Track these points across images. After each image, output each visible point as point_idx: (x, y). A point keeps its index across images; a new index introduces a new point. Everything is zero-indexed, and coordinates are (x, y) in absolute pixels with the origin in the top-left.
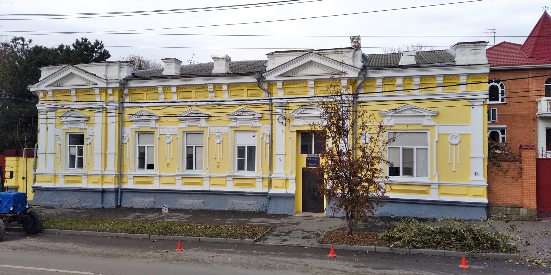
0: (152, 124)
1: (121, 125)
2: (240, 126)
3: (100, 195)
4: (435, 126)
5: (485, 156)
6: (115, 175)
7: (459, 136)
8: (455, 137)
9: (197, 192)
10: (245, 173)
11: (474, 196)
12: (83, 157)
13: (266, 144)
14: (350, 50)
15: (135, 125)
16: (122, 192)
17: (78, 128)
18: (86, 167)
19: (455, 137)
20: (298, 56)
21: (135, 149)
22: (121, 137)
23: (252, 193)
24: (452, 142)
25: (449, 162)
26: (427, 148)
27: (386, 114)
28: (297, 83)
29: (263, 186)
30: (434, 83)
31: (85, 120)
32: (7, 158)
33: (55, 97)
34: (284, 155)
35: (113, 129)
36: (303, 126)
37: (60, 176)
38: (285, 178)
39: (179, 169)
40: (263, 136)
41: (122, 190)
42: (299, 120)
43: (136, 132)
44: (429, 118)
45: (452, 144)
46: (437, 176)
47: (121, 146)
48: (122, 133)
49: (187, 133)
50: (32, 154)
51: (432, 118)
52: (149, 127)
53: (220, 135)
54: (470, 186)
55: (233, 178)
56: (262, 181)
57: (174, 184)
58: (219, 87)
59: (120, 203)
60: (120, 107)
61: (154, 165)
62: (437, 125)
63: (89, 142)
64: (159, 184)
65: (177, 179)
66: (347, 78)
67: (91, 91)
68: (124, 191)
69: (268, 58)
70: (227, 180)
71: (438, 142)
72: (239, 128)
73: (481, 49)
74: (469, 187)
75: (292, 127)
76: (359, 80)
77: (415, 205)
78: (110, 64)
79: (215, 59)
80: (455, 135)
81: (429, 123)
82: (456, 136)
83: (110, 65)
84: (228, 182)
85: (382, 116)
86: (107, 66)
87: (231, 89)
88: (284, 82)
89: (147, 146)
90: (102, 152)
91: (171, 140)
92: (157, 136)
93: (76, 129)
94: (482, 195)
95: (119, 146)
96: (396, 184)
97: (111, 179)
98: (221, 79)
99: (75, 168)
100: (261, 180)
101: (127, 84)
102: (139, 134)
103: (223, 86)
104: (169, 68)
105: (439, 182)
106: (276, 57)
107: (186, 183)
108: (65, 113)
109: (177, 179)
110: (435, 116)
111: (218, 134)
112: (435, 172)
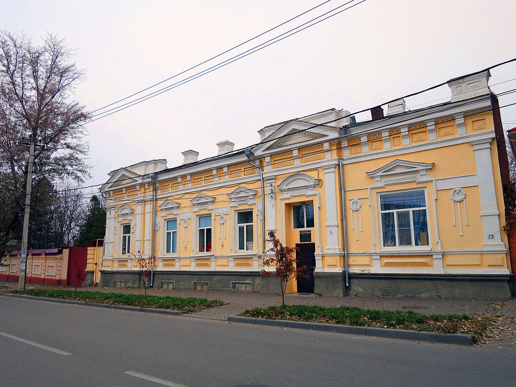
0: (174, 211)
1: (155, 213)
2: (386, 185)
3: (138, 276)
4: (432, 181)
5: (499, 212)
6: (340, 254)
7: (463, 190)
8: (458, 191)
9: (229, 274)
10: (205, 254)
11: (489, 266)
12: (311, 233)
13: (353, 212)
14: (331, 111)
15: (164, 213)
16: (154, 274)
17: (127, 219)
18: (320, 246)
19: (458, 191)
20: (276, 130)
21: (164, 235)
22: (155, 226)
23: (177, 272)
24: (455, 199)
25: (454, 225)
26: (176, 232)
27: (374, 174)
28: (240, 165)
29: (444, 265)
30: (241, 169)
31: (131, 213)
32: (88, 248)
33: (115, 196)
34: (337, 227)
35: (148, 217)
36: (291, 198)
37: (159, 261)
38: (441, 252)
39: (193, 251)
40: (258, 213)
41: (154, 273)
42: (287, 192)
43: (165, 220)
44: (424, 173)
45: (455, 202)
46: (439, 244)
47: (154, 232)
48: (155, 221)
49: (201, 217)
50: (101, 244)
51: (428, 172)
52: (172, 214)
53: (223, 216)
54: (371, 255)
55: (380, 256)
56: (443, 258)
57: (190, 265)
58: (243, 165)
59: (153, 285)
60: (153, 199)
61: (315, 243)
62: (434, 180)
63: (133, 232)
64: (216, 265)
65: (374, 259)
66: (408, 126)
67: (240, 165)
68: (156, 273)
69: (218, 146)
70: (373, 258)
71: (438, 201)
72: (385, 188)
73: (480, 81)
74: (372, 256)
75: (162, 217)
76: (343, 141)
77: (416, 281)
78: (148, 163)
79: (219, 145)
80: (458, 189)
81: (424, 179)
82: (459, 191)
83: (149, 164)
84: (374, 262)
85: (370, 177)
86: (147, 165)
87: (439, 127)
88: (271, 155)
89: (173, 232)
90: (338, 224)
91: (464, 196)
92: (213, 217)
93: (244, 208)
94: (189, 265)
95: (152, 233)
96: (238, 258)
97: (337, 261)
98: (222, 162)
99: (204, 252)
100: (321, 258)
101: (156, 178)
102: (167, 221)
103: (383, 135)
104: (222, 151)
105: (443, 251)
106: (266, 132)
107: (387, 265)
108: (119, 209)
109: (374, 259)
110: (431, 169)
111: (222, 215)
112: (437, 239)
